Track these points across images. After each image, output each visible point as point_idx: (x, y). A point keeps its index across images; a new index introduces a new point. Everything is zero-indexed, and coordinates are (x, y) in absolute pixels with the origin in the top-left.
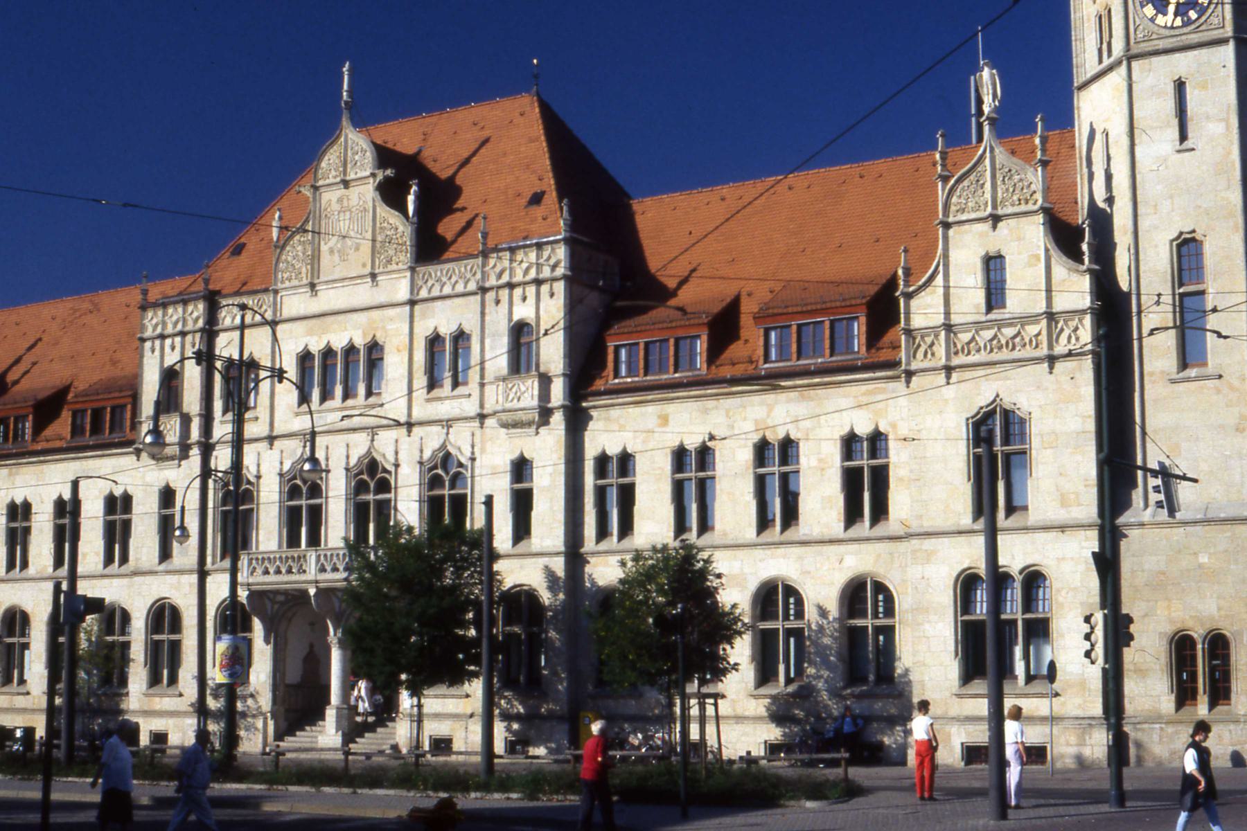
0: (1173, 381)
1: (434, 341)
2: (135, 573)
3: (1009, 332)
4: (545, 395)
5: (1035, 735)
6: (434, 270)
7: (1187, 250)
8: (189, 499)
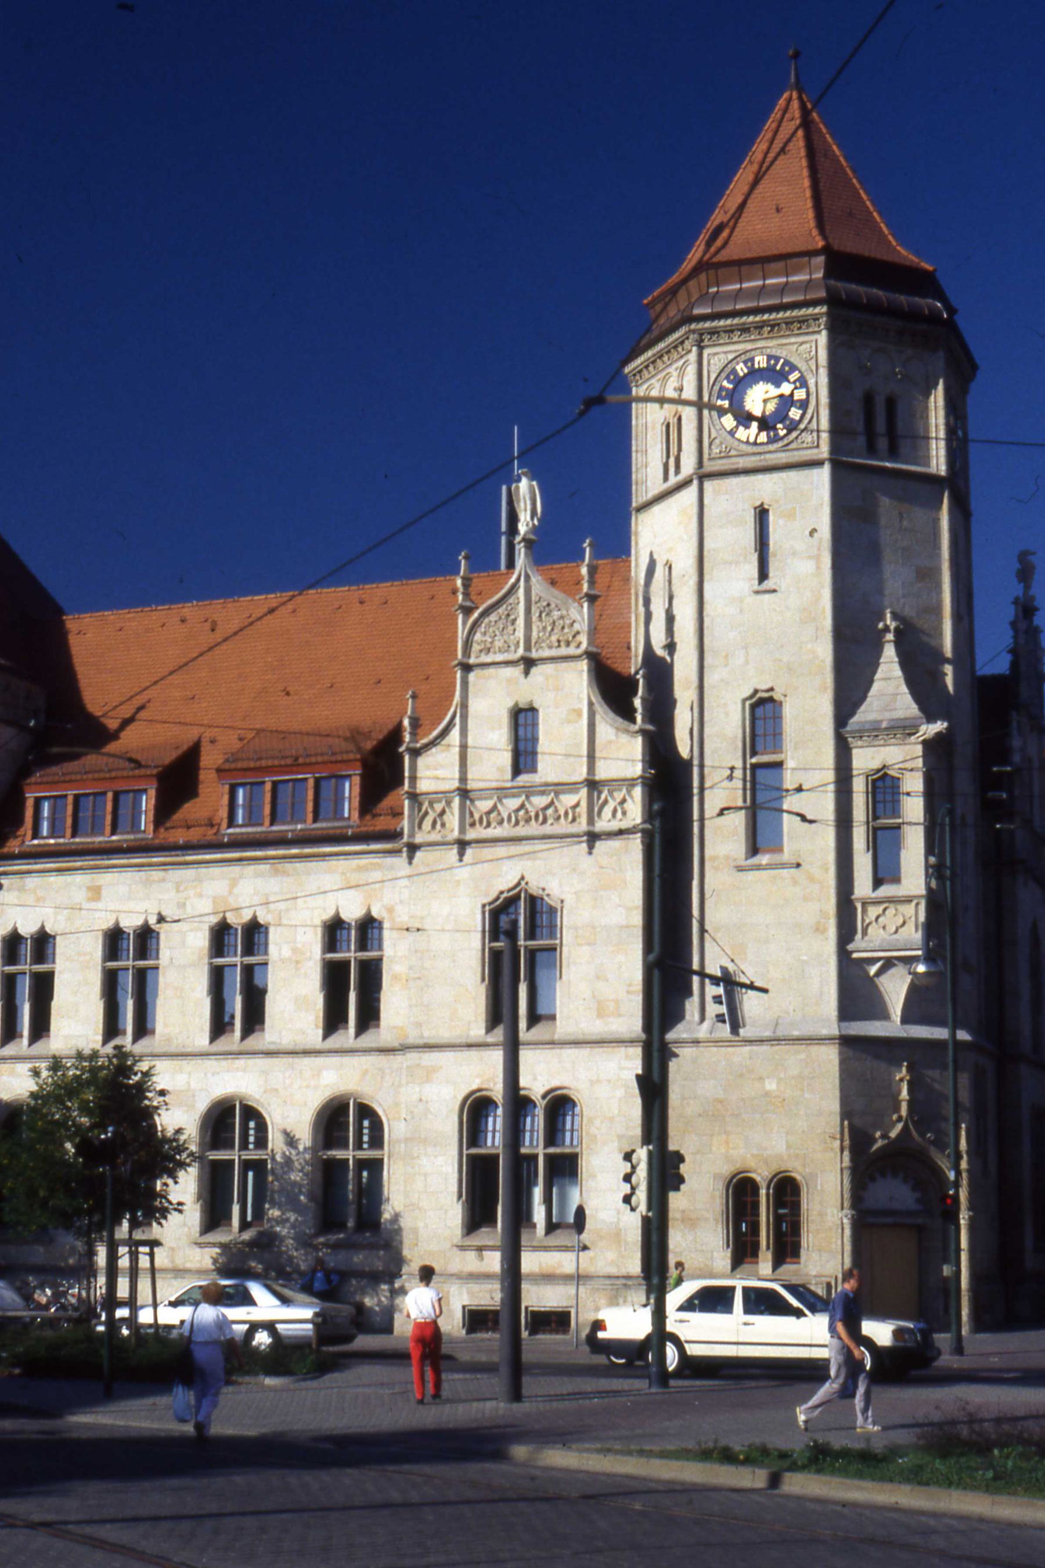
0: (740, 869)
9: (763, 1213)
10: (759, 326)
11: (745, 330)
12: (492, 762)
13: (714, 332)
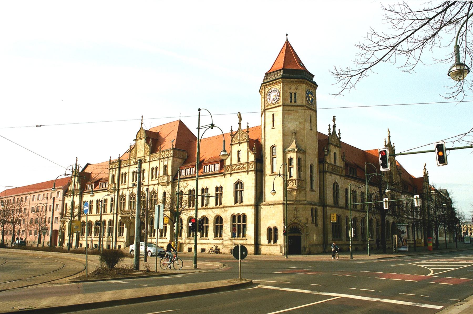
0: (270, 176)
1: (153, 169)
2: (223, 207)
3: (241, 166)
4: (168, 179)
5: (203, 246)
6: (153, 155)
7: (273, 147)
8: (168, 196)
9: (272, 234)
10: (272, 84)
11: (270, 84)
12: (235, 161)
13: (266, 85)
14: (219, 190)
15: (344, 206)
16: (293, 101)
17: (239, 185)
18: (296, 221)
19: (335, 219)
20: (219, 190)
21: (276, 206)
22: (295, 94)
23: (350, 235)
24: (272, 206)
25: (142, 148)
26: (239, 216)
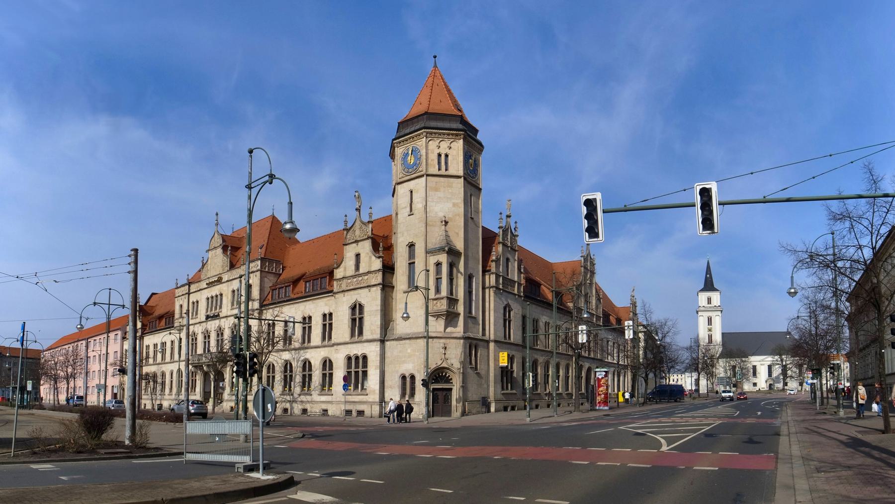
2: (333, 345)
14: (328, 318)
15: (520, 342)
16: (443, 167)
17: (357, 309)
18: (444, 365)
19: (506, 361)
20: (328, 318)
21: (413, 341)
22: (447, 156)
23: (527, 385)
24: (407, 341)
25: (218, 261)
26: (357, 358)
